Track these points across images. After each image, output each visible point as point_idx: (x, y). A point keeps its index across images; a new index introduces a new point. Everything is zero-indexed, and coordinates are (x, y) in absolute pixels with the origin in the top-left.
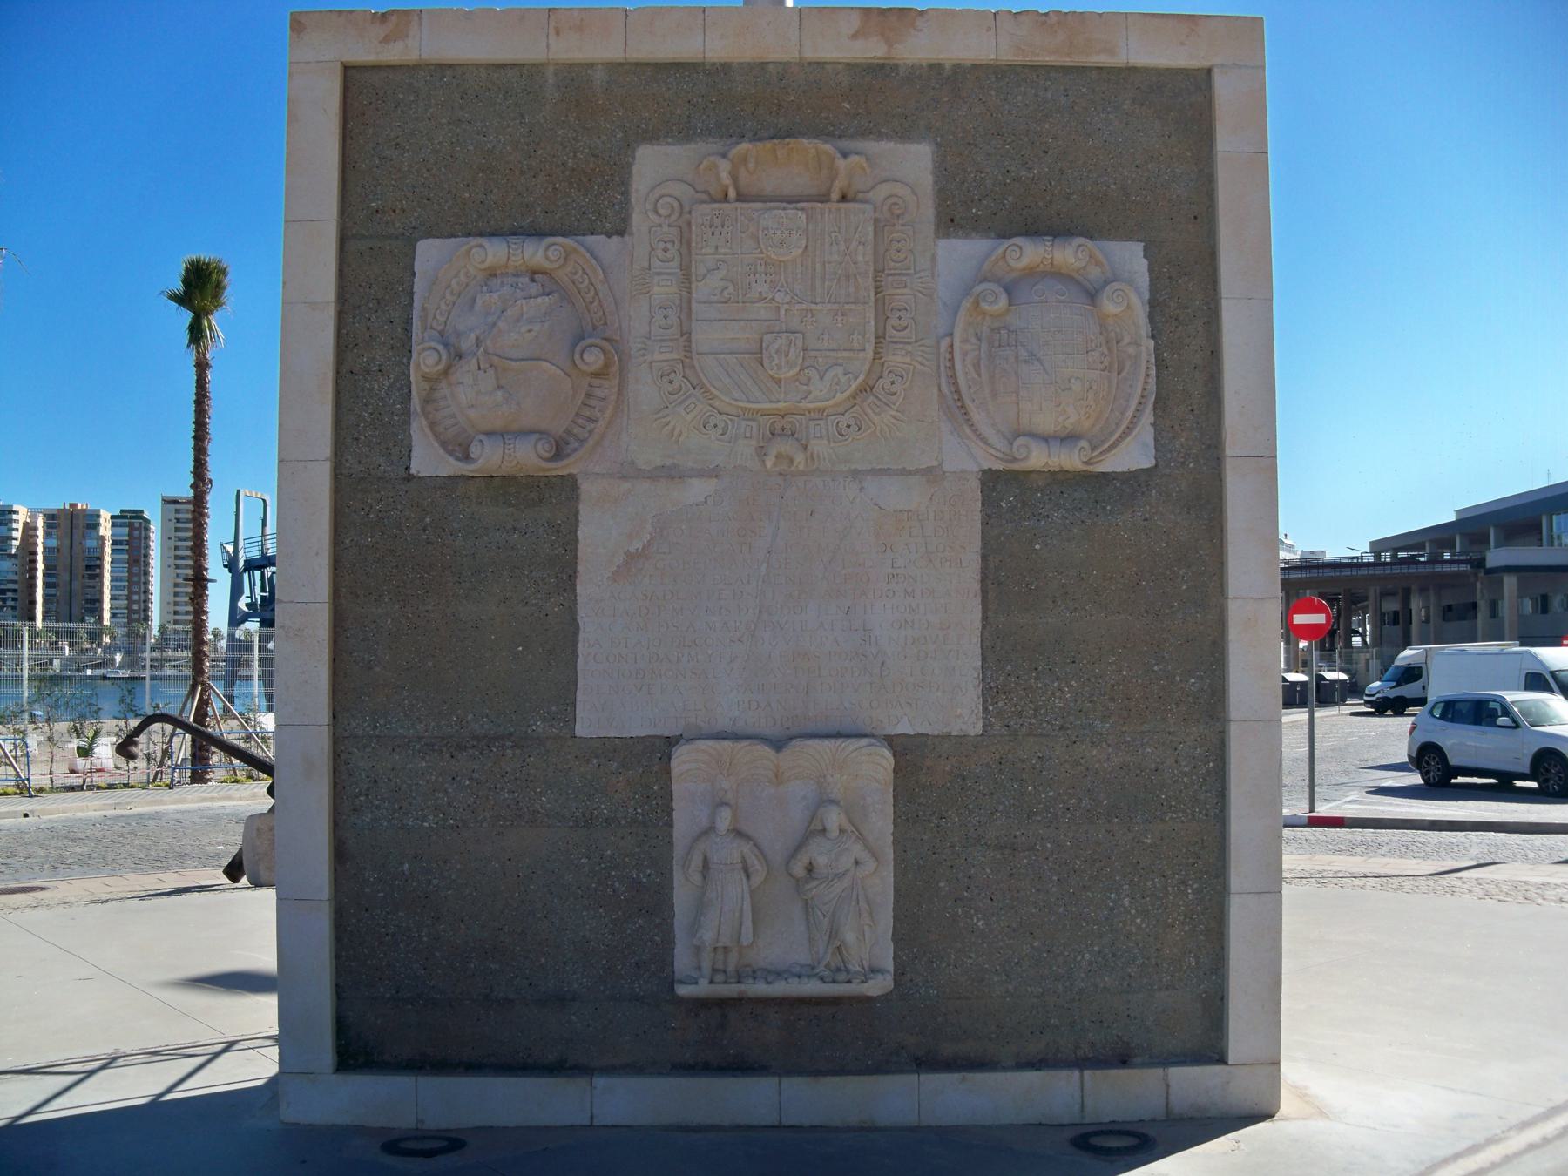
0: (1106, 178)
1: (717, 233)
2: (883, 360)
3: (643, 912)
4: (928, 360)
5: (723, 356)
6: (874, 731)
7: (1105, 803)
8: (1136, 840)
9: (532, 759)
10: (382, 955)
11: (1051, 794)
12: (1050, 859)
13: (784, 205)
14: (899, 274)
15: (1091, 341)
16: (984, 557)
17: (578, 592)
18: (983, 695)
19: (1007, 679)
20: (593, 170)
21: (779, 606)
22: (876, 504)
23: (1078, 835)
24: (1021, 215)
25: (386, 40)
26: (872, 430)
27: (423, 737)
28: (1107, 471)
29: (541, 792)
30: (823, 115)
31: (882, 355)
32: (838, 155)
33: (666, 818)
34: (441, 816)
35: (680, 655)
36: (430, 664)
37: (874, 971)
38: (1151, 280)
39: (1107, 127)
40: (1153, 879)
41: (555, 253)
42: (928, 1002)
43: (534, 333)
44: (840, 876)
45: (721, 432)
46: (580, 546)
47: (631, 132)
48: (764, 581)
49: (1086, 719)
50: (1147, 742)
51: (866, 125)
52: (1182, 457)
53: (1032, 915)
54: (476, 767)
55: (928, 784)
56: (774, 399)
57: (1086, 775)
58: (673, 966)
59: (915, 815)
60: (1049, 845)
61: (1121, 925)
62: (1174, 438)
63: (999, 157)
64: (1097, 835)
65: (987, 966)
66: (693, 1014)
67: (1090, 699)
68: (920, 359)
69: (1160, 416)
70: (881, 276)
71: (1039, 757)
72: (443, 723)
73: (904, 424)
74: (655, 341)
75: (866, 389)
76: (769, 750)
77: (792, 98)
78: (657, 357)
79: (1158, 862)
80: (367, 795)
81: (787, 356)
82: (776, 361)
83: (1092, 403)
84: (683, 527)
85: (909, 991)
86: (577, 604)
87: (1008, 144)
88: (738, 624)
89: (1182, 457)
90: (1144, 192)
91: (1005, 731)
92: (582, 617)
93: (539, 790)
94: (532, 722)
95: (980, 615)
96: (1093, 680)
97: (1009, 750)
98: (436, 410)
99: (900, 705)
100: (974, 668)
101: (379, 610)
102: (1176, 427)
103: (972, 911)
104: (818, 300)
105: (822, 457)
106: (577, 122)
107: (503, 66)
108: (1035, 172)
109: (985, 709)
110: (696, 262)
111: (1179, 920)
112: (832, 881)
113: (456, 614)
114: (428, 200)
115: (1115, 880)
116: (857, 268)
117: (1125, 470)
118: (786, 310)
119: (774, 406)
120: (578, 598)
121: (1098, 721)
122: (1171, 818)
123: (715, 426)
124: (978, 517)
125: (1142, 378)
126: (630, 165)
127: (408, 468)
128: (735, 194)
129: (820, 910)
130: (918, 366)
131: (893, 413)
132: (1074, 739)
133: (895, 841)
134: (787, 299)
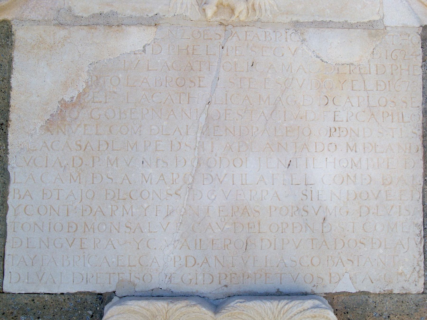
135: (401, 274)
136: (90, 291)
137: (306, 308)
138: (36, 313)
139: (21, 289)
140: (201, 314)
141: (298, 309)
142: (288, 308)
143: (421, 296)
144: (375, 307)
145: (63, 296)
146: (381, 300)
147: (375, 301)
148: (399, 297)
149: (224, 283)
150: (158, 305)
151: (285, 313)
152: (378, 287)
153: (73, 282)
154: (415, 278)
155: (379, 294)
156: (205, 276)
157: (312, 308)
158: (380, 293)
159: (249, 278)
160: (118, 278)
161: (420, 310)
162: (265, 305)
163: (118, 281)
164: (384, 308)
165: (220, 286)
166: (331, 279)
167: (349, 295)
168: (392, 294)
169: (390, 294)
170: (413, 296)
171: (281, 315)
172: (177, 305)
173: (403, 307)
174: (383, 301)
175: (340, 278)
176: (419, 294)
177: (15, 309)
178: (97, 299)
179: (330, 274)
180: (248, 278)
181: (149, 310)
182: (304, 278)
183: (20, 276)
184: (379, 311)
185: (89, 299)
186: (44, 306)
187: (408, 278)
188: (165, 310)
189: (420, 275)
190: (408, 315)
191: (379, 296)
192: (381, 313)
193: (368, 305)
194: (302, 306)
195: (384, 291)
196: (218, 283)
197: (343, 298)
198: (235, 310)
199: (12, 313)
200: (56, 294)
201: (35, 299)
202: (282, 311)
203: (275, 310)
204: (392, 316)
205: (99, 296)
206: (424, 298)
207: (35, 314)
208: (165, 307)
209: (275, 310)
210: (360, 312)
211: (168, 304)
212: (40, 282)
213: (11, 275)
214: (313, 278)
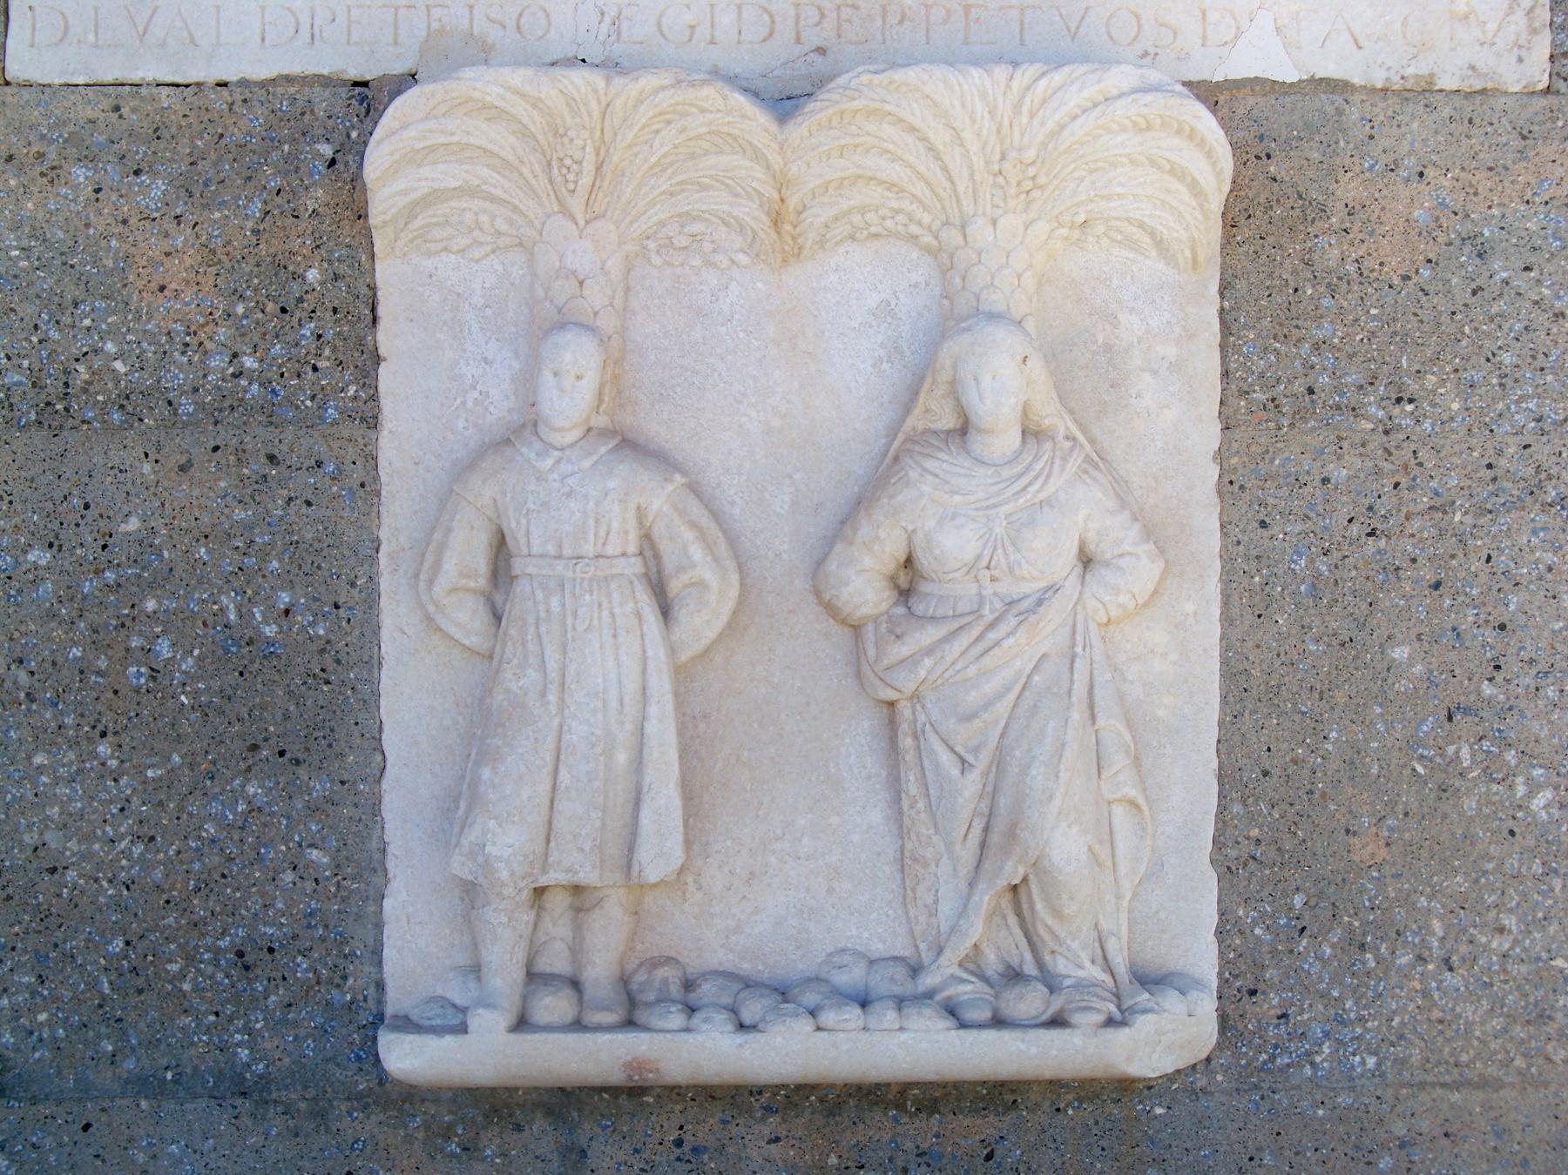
33: (352, 390)
42: (1344, 1099)
55: (1351, 268)
59: (1299, 387)
103: (1511, 756)
112: (992, 626)
133: (1229, 487)
135: (1466, 17)
136: (325, 72)
137: (1115, 92)
138: (128, 156)
139: (71, 68)
140: (730, 119)
141: (1086, 94)
142: (1050, 91)
143: (1541, 103)
144: (1371, 137)
145: (225, 92)
146: (1390, 113)
147: (1369, 117)
148: (1457, 105)
149: (813, 38)
150: (572, 83)
151: (1039, 110)
152: (1379, 62)
153: (263, 40)
154: (1518, 34)
155: (1385, 90)
156: (745, 15)
157: (1135, 91)
158: (1388, 85)
159: (907, 23)
160: (425, 24)
161: (1538, 154)
162: (964, 77)
163: (424, 34)
164: (1405, 143)
165: (797, 50)
166: (1205, 31)
167: (1273, 90)
168: (1431, 92)
169: (1423, 93)
170: (1511, 101)
171: (1024, 120)
172: (642, 82)
173: (1474, 141)
174: (1399, 118)
175: (1238, 28)
176: (1533, 93)
177: (51, 142)
178: (349, 99)
179: (1204, 14)
180: (901, 22)
181: (541, 105)
182: (1107, 25)
183: (66, 22)
184: (1384, 151)
185: (322, 101)
186: (156, 130)
187: (1490, 35)
188: (599, 102)
189: (1537, 25)
190: (1491, 169)
191: (1385, 99)
192: (1391, 159)
193: (1344, 131)
194: (1099, 82)
195: (1403, 78)
196: (793, 41)
197: (1251, 101)
198: (854, 99)
199: (41, 156)
200: (199, 84)
201: (122, 104)
202: (1028, 100)
203: (1000, 100)
204: (1432, 174)
205: (358, 90)
206: (1552, 111)
207: (124, 156)
208: (595, 91)
209: (1000, 100)
210: (1316, 156)
211: (608, 80)
212: (141, 41)
213: (34, 17)
214: (1140, 27)
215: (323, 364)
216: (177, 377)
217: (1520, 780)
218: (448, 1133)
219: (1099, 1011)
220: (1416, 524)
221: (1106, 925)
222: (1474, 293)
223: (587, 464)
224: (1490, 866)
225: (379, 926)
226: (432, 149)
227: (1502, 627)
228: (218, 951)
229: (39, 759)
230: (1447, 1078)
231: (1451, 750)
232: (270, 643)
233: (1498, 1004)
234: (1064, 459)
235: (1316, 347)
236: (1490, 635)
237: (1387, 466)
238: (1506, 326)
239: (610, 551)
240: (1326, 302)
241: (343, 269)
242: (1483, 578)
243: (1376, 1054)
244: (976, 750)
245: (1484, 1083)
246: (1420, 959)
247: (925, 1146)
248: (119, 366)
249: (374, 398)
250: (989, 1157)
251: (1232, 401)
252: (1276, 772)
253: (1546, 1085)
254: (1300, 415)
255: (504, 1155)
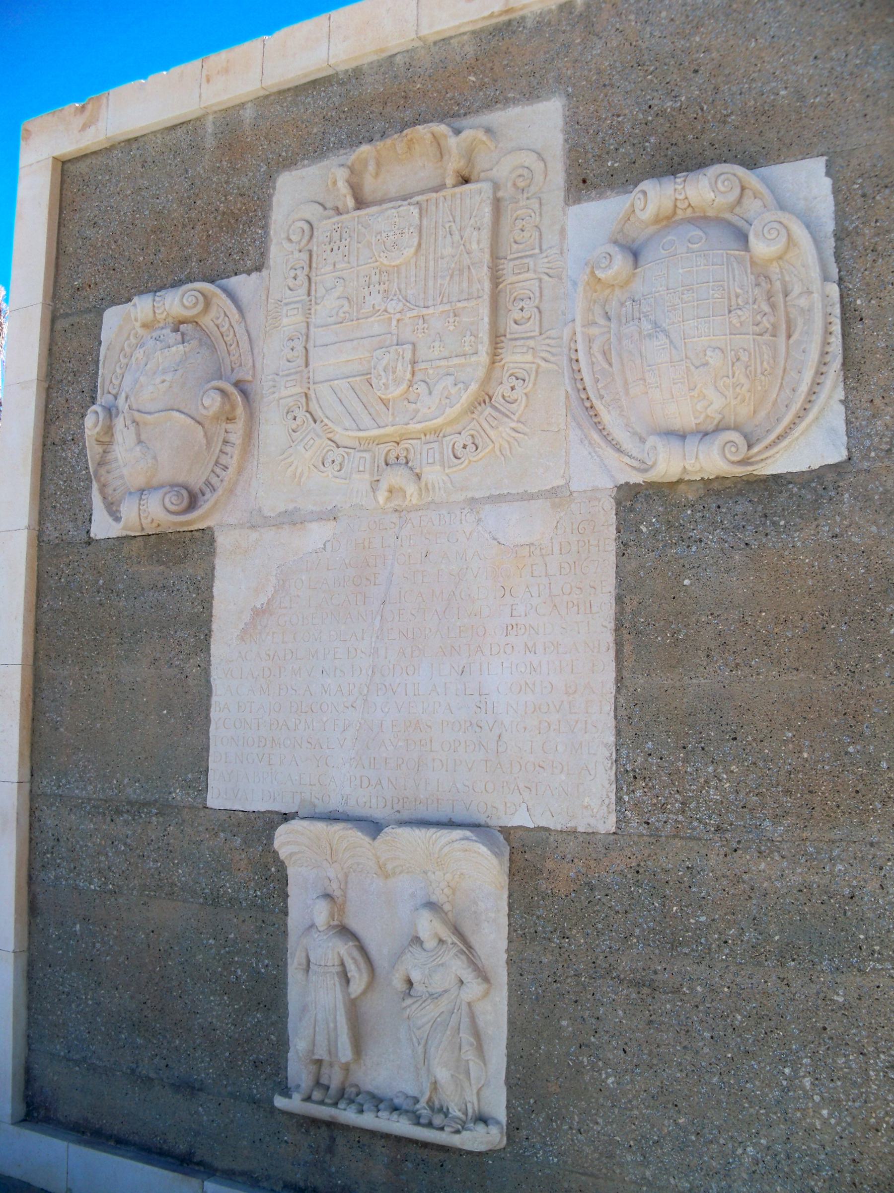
0: (774, 84)
1: (335, 248)
2: (503, 363)
3: (261, 1005)
4: (553, 355)
5: (336, 382)
6: (488, 820)
7: (777, 938)
8: (822, 995)
9: (172, 828)
10: (59, 1013)
11: (703, 919)
12: (701, 1008)
13: (400, 203)
14: (521, 257)
15: (737, 297)
16: (619, 599)
17: (212, 652)
18: (617, 780)
19: (647, 760)
20: (240, 210)
21: (391, 666)
22: (494, 539)
23: (738, 980)
24: (666, 156)
25: (85, 127)
26: (490, 448)
27: (93, 799)
28: (779, 472)
29: (178, 863)
30: (448, 95)
31: (502, 356)
32: (451, 133)
33: (282, 904)
34: (103, 879)
35: (298, 722)
36: (98, 725)
37: (483, 1119)
38: (837, 204)
39: (775, 18)
40: (845, 1056)
41: (190, 300)
42: (547, 1171)
43: (166, 384)
44: (434, 997)
45: (338, 468)
46: (215, 603)
47: (273, 163)
48: (377, 637)
49: (751, 819)
50: (839, 856)
51: (492, 94)
52: (886, 443)
53: (676, 1080)
54: (129, 833)
55: (549, 892)
56: (382, 424)
57: (750, 897)
58: (286, 1071)
59: (532, 930)
60: (699, 989)
61: (799, 1114)
62: (874, 416)
63: (639, 92)
64: (766, 982)
65: (618, 1138)
66: (303, 1130)
67: (756, 791)
68: (544, 355)
69: (853, 388)
70: (504, 264)
71: (688, 868)
72: (107, 785)
73: (526, 437)
74: (283, 376)
75: (484, 399)
76: (363, 837)
77: (418, 86)
78: (285, 393)
79: (854, 1031)
80: (52, 853)
81: (394, 372)
82: (384, 380)
83: (743, 380)
84: (303, 578)
85: (525, 1152)
86: (210, 665)
87: (651, 74)
88: (351, 687)
89: (886, 443)
90: (826, 90)
91: (643, 829)
92: (215, 679)
93: (176, 862)
94: (172, 789)
95: (614, 675)
96: (761, 764)
97: (649, 856)
98: (108, 472)
99: (518, 789)
100: (606, 745)
101: (66, 672)
102: (878, 401)
103: (600, 1063)
104: (430, 303)
105: (436, 485)
106: (229, 165)
107: (174, 127)
108: (683, 99)
109: (619, 799)
110: (316, 283)
111: (887, 1123)
112: (424, 1001)
113: (118, 676)
114: (114, 270)
115: (790, 1049)
116: (470, 259)
117: (804, 469)
118: (398, 321)
119: (381, 431)
120: (211, 658)
121: (767, 823)
122: (874, 969)
123: (333, 462)
124: (612, 547)
125: (817, 338)
126: (270, 196)
127: (88, 532)
128: (353, 201)
129: (414, 1034)
130: (543, 364)
131: (513, 425)
132: (735, 845)
133: (510, 962)
134: (399, 309)
149: (396, 808)
197: (520, 833)
199: (213, 829)
215: (275, 896)
216: (242, 896)
217: (603, 1072)
218: (302, 1126)
219: (452, 1127)
220: (569, 980)
221: (468, 1099)
222: (589, 902)
223: (325, 937)
224: (593, 1100)
225: (287, 1060)
226: (288, 842)
227: (598, 1018)
228: (250, 1060)
229: (212, 998)
230: (580, 1171)
231: (581, 1058)
232: (263, 974)
233: (597, 1149)
234: (449, 951)
235: (538, 917)
236: (594, 1021)
237: (560, 959)
238: (599, 915)
239: (328, 964)
240: (542, 902)
241: (280, 869)
242: (592, 1000)
243: (556, 1157)
244: (421, 1039)
245: (592, 1175)
246: (571, 1128)
247: (424, 1158)
248: (229, 890)
249: (287, 907)
250: (442, 1166)
251: (512, 933)
252: (525, 1057)
253: (614, 1180)
254: (533, 939)
255: (315, 1135)
